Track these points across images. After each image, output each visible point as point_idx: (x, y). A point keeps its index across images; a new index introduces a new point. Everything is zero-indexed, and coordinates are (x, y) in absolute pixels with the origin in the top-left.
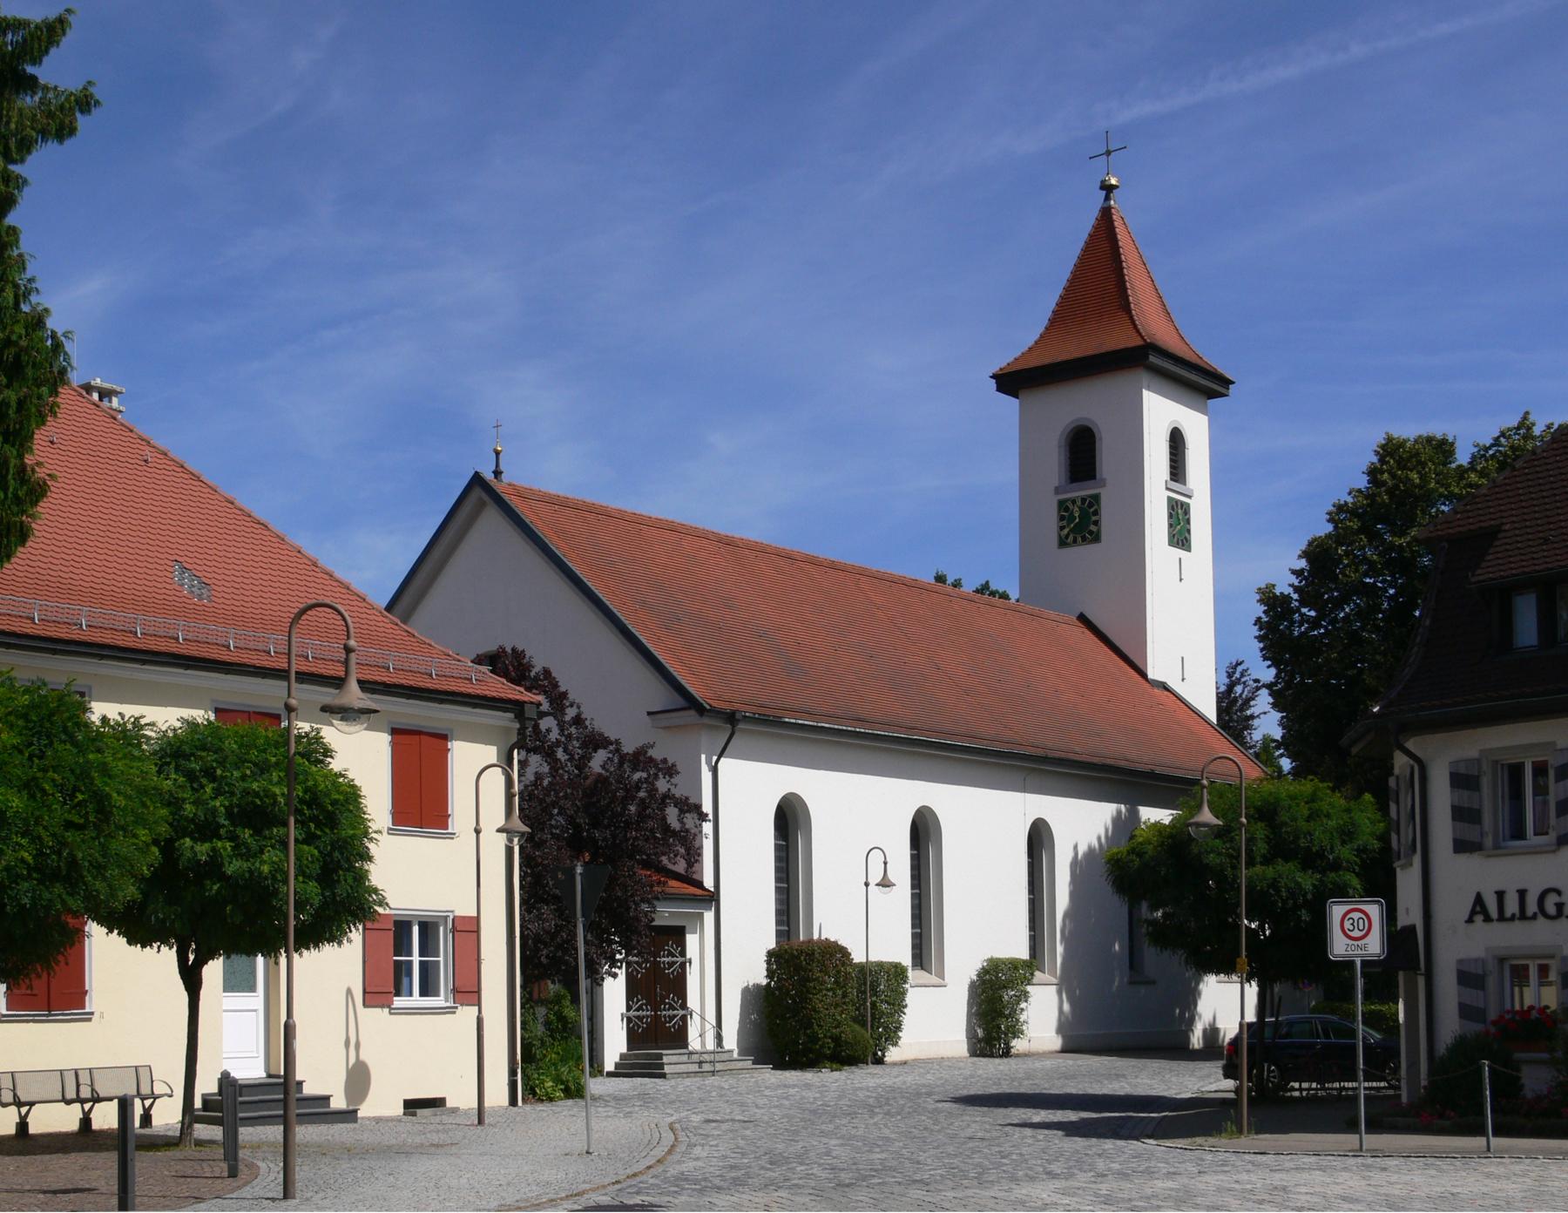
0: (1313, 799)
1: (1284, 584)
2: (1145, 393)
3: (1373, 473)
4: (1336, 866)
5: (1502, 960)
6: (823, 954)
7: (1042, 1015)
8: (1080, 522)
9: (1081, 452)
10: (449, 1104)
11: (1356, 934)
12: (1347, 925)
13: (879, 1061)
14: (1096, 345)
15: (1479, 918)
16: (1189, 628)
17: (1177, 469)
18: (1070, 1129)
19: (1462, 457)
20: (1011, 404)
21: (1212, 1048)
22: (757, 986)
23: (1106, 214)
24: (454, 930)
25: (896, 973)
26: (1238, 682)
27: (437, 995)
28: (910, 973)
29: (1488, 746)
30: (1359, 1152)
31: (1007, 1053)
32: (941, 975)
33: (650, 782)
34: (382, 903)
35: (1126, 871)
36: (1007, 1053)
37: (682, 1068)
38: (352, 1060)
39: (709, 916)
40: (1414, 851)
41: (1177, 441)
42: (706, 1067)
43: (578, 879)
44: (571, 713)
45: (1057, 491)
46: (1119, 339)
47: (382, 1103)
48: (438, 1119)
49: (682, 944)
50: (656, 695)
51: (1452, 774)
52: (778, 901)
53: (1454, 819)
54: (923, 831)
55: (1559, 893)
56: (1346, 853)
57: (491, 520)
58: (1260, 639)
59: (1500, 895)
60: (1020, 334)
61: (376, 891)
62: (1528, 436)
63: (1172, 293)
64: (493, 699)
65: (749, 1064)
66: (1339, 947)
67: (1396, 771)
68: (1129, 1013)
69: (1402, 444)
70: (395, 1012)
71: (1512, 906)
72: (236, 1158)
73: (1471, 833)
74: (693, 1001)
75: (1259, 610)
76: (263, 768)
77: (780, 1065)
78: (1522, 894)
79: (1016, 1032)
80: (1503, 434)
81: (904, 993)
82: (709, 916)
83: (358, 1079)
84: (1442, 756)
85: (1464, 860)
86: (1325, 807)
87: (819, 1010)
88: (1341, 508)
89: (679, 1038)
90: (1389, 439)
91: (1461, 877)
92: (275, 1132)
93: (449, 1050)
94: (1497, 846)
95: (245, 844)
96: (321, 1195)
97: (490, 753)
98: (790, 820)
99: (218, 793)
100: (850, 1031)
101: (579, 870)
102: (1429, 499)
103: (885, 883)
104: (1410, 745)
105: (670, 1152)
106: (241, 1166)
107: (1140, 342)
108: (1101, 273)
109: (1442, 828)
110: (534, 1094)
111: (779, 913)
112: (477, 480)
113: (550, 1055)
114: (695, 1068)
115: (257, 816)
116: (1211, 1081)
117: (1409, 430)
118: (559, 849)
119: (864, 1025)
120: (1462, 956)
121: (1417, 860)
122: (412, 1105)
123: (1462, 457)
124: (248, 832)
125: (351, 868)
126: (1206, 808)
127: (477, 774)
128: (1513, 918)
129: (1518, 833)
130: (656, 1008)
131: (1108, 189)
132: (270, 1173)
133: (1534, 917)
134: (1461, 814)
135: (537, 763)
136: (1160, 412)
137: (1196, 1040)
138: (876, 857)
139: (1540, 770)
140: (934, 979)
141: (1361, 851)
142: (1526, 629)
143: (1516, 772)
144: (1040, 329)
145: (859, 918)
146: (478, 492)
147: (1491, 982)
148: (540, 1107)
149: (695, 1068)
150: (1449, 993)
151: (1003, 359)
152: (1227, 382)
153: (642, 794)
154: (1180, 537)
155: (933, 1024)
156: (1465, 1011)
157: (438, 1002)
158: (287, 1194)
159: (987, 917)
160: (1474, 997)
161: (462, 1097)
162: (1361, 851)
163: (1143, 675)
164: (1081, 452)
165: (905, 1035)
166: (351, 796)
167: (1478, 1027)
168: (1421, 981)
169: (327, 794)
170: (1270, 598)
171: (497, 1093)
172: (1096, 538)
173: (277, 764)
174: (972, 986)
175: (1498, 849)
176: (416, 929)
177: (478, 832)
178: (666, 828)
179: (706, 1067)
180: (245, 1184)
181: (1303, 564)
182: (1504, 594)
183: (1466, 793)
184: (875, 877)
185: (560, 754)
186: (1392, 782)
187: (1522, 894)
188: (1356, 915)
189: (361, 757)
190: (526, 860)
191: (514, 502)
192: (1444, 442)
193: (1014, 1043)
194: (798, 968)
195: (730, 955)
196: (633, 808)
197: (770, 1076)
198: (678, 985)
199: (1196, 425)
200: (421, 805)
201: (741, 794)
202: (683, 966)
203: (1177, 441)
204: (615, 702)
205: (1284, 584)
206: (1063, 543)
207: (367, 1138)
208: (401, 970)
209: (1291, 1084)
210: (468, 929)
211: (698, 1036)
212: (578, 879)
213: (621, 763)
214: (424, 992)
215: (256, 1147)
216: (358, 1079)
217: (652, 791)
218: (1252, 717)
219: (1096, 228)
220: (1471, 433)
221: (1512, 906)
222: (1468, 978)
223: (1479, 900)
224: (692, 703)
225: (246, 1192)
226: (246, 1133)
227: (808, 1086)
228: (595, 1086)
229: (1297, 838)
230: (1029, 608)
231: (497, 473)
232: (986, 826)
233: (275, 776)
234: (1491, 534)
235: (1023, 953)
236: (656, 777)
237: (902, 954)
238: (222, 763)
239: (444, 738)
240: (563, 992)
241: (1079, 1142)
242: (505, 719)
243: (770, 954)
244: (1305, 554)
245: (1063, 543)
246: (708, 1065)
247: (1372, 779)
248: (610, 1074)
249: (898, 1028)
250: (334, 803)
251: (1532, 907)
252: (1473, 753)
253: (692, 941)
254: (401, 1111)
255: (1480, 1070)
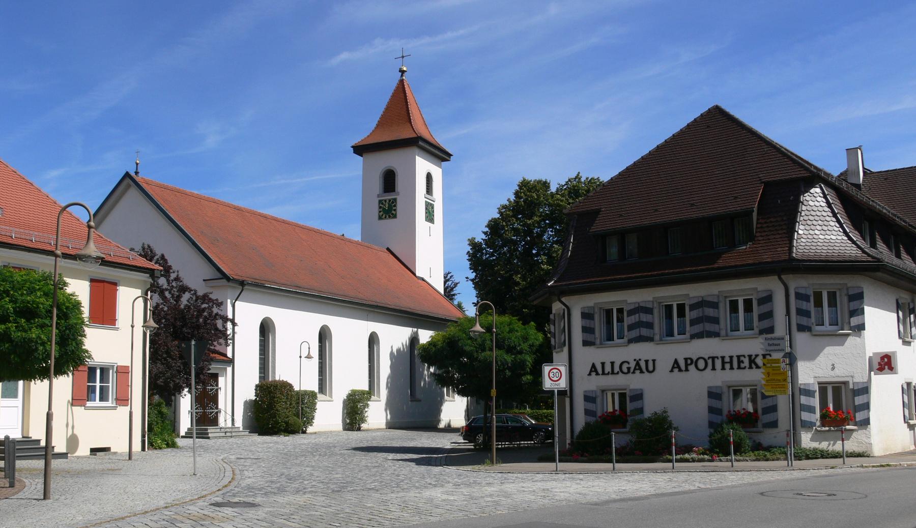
0: (510, 324)
1: (480, 237)
2: (417, 157)
3: (517, 194)
4: (520, 352)
5: (729, 387)
6: (281, 387)
7: (377, 415)
8: (388, 210)
9: (389, 181)
10: (112, 450)
11: (555, 379)
12: (551, 375)
13: (304, 432)
14: (396, 137)
15: (593, 374)
16: (436, 254)
17: (429, 190)
18: (418, 462)
19: (553, 189)
20: (359, 159)
21: (449, 429)
22: (251, 401)
23: (402, 82)
24: (117, 372)
25: (313, 395)
26: (448, 280)
27: (107, 400)
28: (318, 395)
29: (657, 295)
30: (556, 471)
31: (359, 429)
32: (331, 396)
33: (210, 308)
34: (90, 357)
35: (414, 354)
36: (359, 429)
37: (217, 435)
38: (70, 433)
39: (229, 369)
40: (565, 345)
41: (429, 178)
42: (228, 434)
43: (193, 347)
44: (173, 276)
45: (378, 196)
46: (407, 134)
47: (83, 450)
48: (107, 457)
49: (217, 381)
50: (207, 272)
51: (582, 313)
52: (260, 364)
53: (583, 331)
54: (324, 336)
55: (628, 363)
56: (525, 346)
57: (133, 193)
58: (469, 260)
59: (603, 364)
60: (365, 128)
61: (87, 351)
62: (579, 182)
63: (428, 118)
64: (140, 267)
65: (247, 433)
66: (548, 384)
67: (554, 312)
68: (415, 412)
69: (529, 182)
70: (87, 408)
71: (608, 368)
72: (14, 478)
73: (590, 338)
74: (221, 405)
75: (469, 248)
76: (32, 291)
77: (262, 433)
78: (612, 363)
79: (363, 420)
80: (569, 180)
81: (316, 404)
82: (229, 369)
83: (73, 442)
84: (578, 304)
85: (590, 350)
86: (516, 328)
87: (277, 411)
88: (504, 207)
89: (214, 422)
90: (524, 180)
91: (585, 356)
92: (41, 463)
93: (113, 426)
94: (601, 344)
95: (22, 326)
96: (63, 497)
97: (138, 292)
98: (266, 329)
99: (10, 301)
100: (292, 419)
101: (193, 343)
102: (539, 204)
103: (309, 357)
104: (563, 299)
105: (234, 474)
106: (17, 483)
107: (415, 136)
108: (399, 105)
109: (578, 336)
110: (152, 445)
111: (260, 368)
112: (127, 175)
113: (159, 430)
114: (223, 434)
115: (29, 313)
116: (458, 441)
117: (532, 177)
118: (167, 337)
119: (298, 417)
120: (711, 385)
121: (566, 349)
122: (94, 451)
123: (553, 189)
124: (23, 320)
125: (75, 339)
126: (478, 324)
127: (130, 302)
128: (608, 374)
129: (670, 334)
130: (204, 409)
131: (403, 72)
132: (34, 486)
133: (618, 373)
134: (585, 330)
135: (157, 298)
136: (423, 165)
137: (442, 425)
138: (305, 346)
139: (620, 311)
140: (328, 398)
141: (531, 346)
142: (613, 251)
143: (609, 313)
144: (375, 125)
145: (295, 370)
146: (128, 180)
147: (725, 398)
148: (156, 452)
149: (223, 434)
150: (580, 405)
151: (358, 138)
152: (450, 155)
153: (205, 314)
154: (430, 217)
155: (328, 417)
156: (587, 412)
157: (108, 404)
158: (46, 496)
159: (349, 374)
160: (591, 406)
161: (120, 446)
162: (531, 346)
163: (414, 274)
164: (389, 181)
165: (316, 421)
166: (78, 305)
167: (594, 419)
168: (567, 400)
169: (64, 304)
170: (474, 245)
171: (137, 446)
172: (395, 216)
173: (39, 289)
174: (344, 402)
175: (602, 345)
176: (98, 371)
177: (133, 327)
178: (217, 329)
179: (228, 434)
180: (19, 491)
181: (487, 229)
182: (603, 237)
183: (588, 321)
184: (305, 354)
185: (167, 294)
186: (552, 317)
187: (612, 363)
188: (555, 371)
189: (79, 289)
190: (152, 342)
191: (144, 186)
192: (545, 183)
193: (362, 425)
194: (270, 392)
195: (238, 387)
196: (201, 320)
197: (257, 438)
198: (214, 399)
199: (437, 173)
200: (105, 314)
201: (246, 315)
202: (217, 390)
203: (429, 178)
204: (192, 273)
205: (480, 237)
206: (380, 218)
207: (76, 466)
208: (91, 390)
209: (485, 444)
210: (124, 372)
211: (224, 420)
212: (193, 347)
213: (196, 300)
214: (101, 399)
215: (30, 471)
216: (73, 442)
217: (210, 314)
218: (454, 295)
219: (397, 88)
220: (557, 180)
221: (608, 368)
222: (588, 398)
223: (593, 366)
224: (224, 276)
225: (21, 495)
226: (19, 464)
227: (276, 443)
228: (180, 442)
229: (504, 340)
230: (366, 244)
231: (137, 173)
232: (350, 333)
233: (39, 294)
234: (597, 212)
235: (366, 388)
236: (213, 307)
237: (316, 389)
238: (13, 288)
239: (115, 284)
240: (162, 401)
241: (423, 468)
242: (145, 277)
243: (257, 386)
244: (488, 226)
245: (380, 218)
246: (230, 433)
247: (541, 317)
248: (183, 437)
249: (313, 418)
250: (67, 308)
251: (617, 369)
252: (591, 304)
253: (221, 380)
254: (89, 453)
255: (611, 436)
